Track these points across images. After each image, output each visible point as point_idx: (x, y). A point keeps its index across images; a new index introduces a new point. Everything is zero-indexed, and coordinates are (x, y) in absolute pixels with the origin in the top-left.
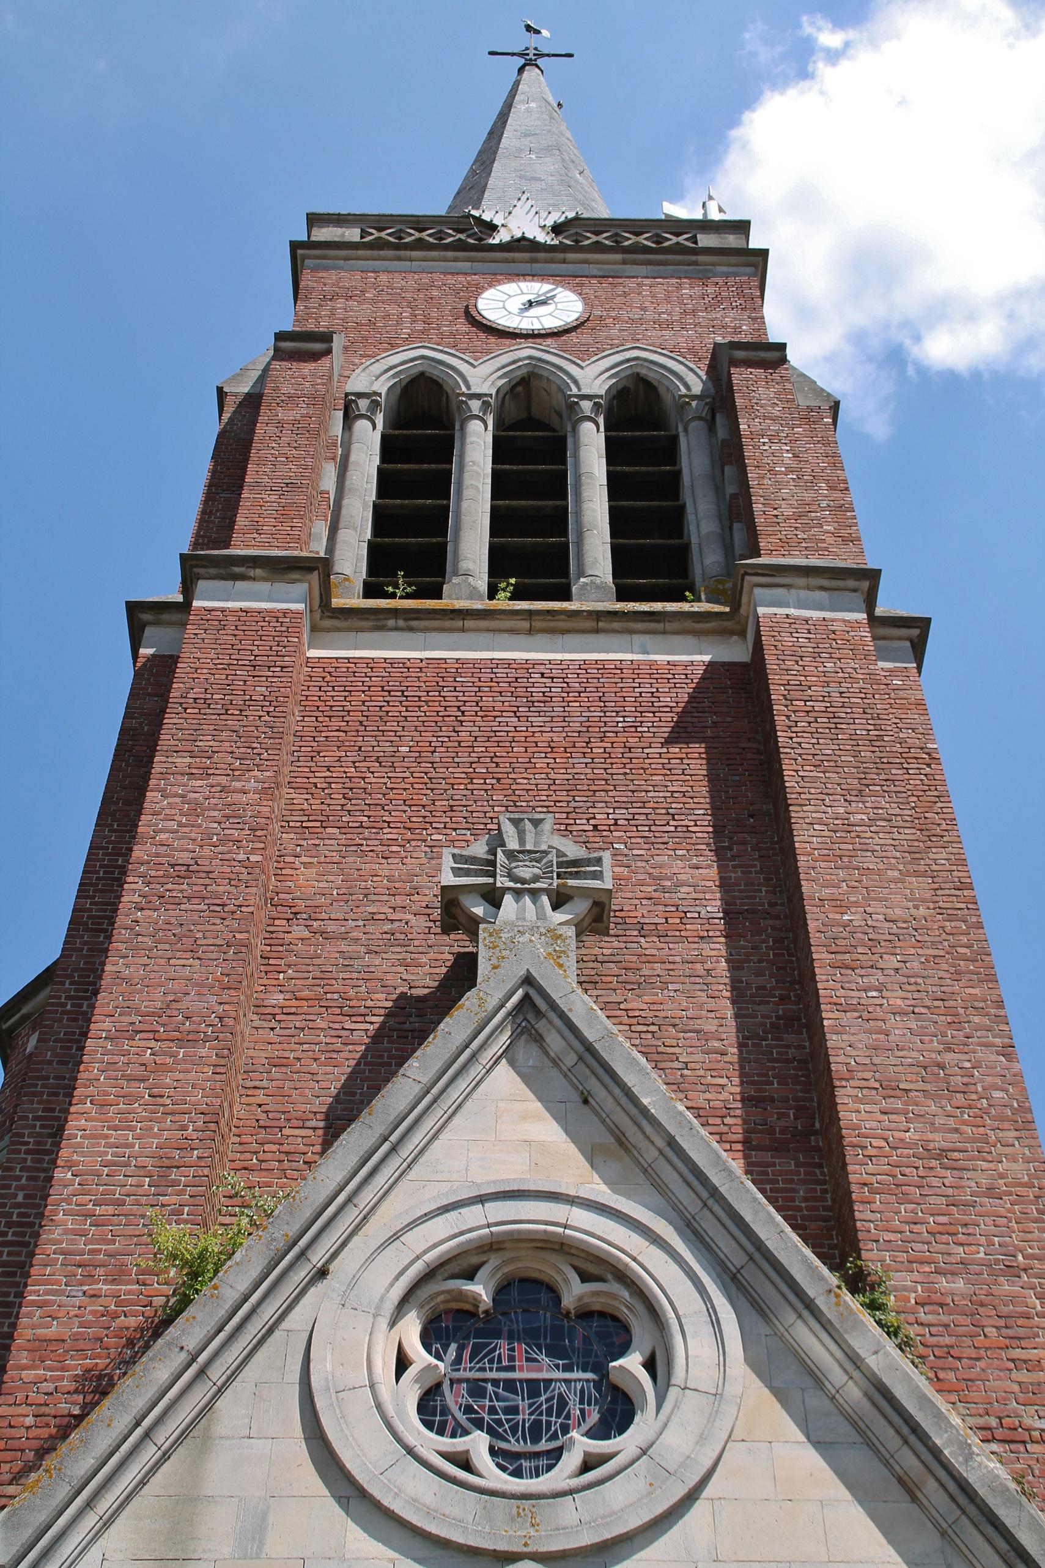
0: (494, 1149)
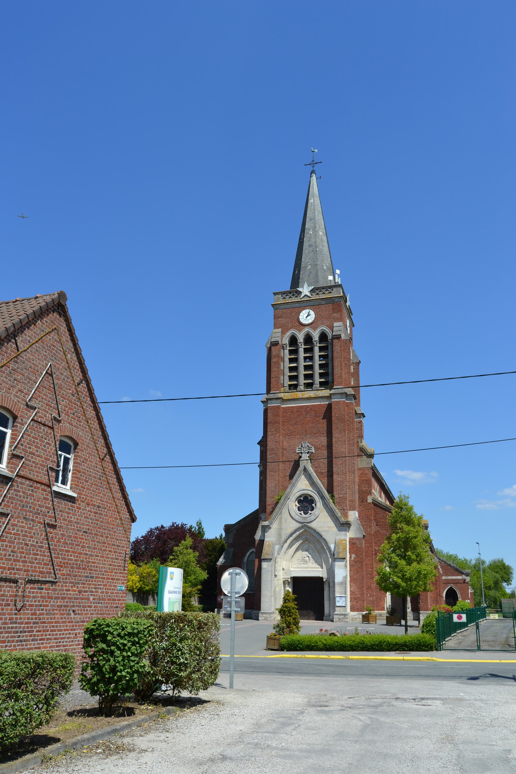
0: (302, 485)
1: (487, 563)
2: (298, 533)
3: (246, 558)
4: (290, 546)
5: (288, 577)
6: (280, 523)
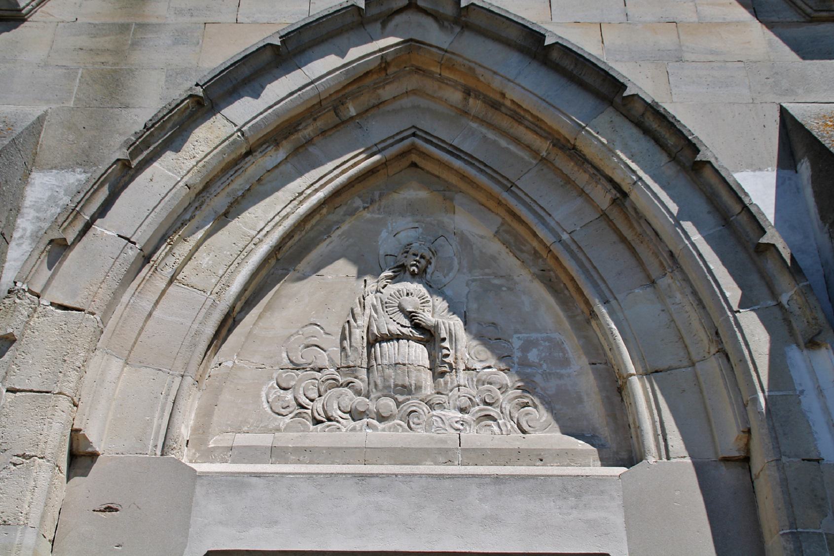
2: (323, 67)
4: (216, 198)
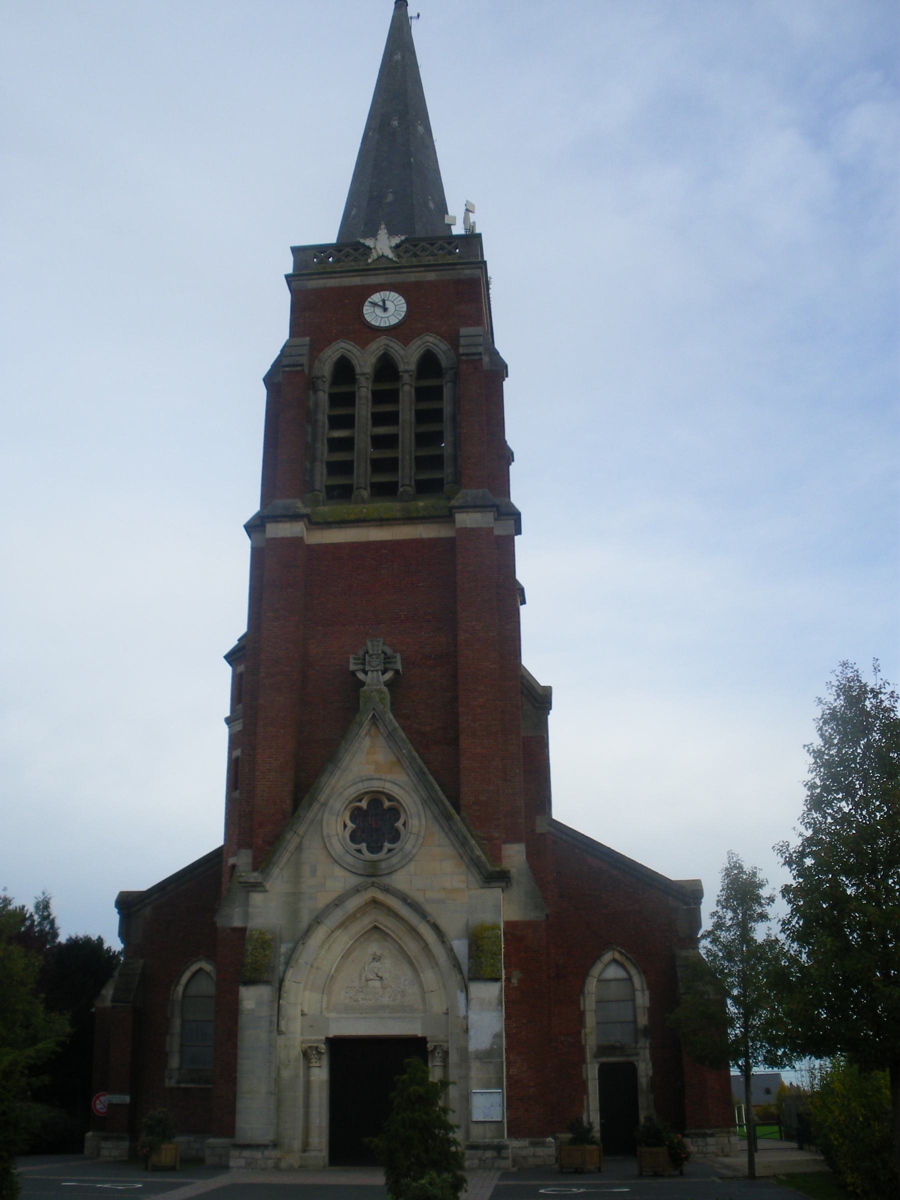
1: (62, 939)
3: (180, 989)
4: (352, 918)
5: (318, 1037)
6: (296, 878)
